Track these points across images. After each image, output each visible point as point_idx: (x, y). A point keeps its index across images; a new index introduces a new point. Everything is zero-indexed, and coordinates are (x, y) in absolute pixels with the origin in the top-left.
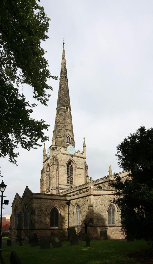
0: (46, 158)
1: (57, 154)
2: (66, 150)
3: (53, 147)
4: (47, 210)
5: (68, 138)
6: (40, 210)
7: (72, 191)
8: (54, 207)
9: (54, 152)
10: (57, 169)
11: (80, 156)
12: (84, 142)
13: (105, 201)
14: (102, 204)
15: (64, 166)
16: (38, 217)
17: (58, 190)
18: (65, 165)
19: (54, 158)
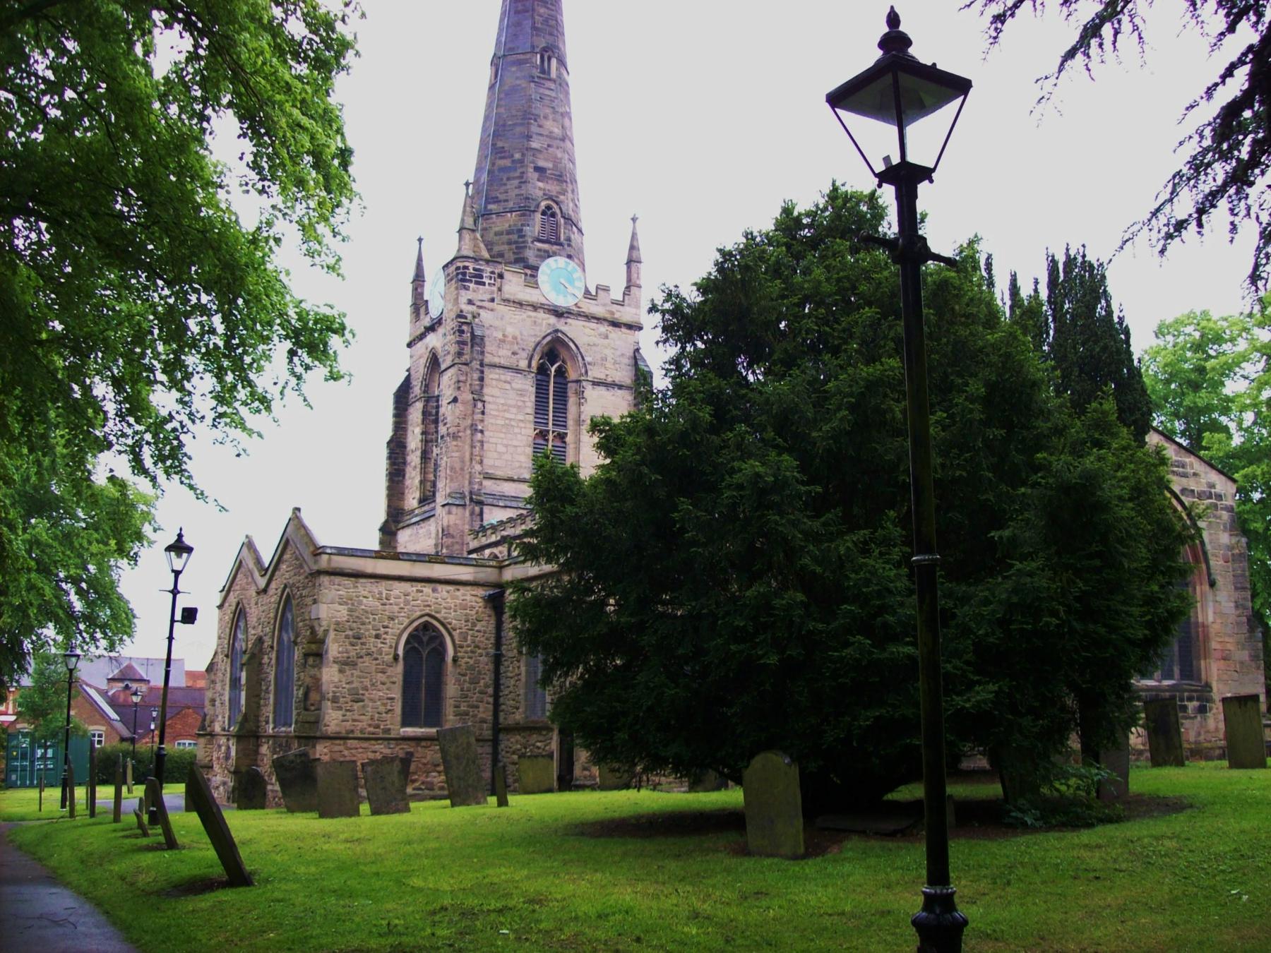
0: (426, 322)
1: (480, 307)
3: (458, 268)
4: (386, 633)
8: (426, 618)
9: (463, 292)
11: (608, 316)
15: (517, 370)
17: (477, 509)
18: (523, 364)
19: (465, 328)
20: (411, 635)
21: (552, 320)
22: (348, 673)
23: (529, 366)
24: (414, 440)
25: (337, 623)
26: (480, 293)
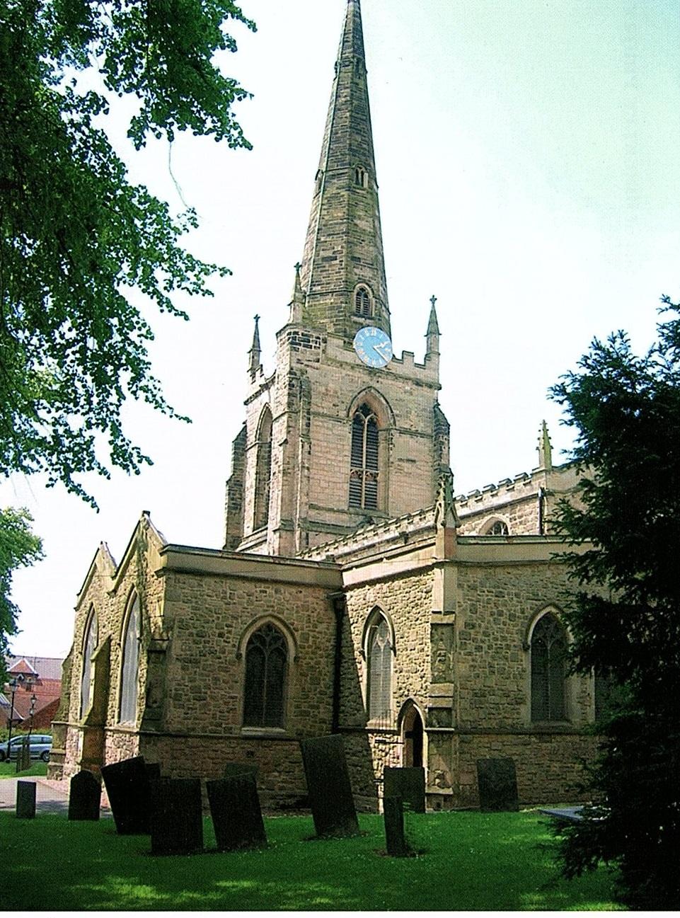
0: (262, 381)
2: (348, 345)
4: (230, 632)
5: (362, 298)
6: (194, 631)
7: (366, 543)
10: (305, 432)
12: (433, 313)
13: (516, 595)
14: (501, 613)
15: (338, 419)
16: (183, 669)
18: (343, 414)
20: (254, 635)
21: (366, 378)
22: (191, 670)
23: (348, 416)
24: (250, 481)
25: (181, 621)
26: (308, 354)
